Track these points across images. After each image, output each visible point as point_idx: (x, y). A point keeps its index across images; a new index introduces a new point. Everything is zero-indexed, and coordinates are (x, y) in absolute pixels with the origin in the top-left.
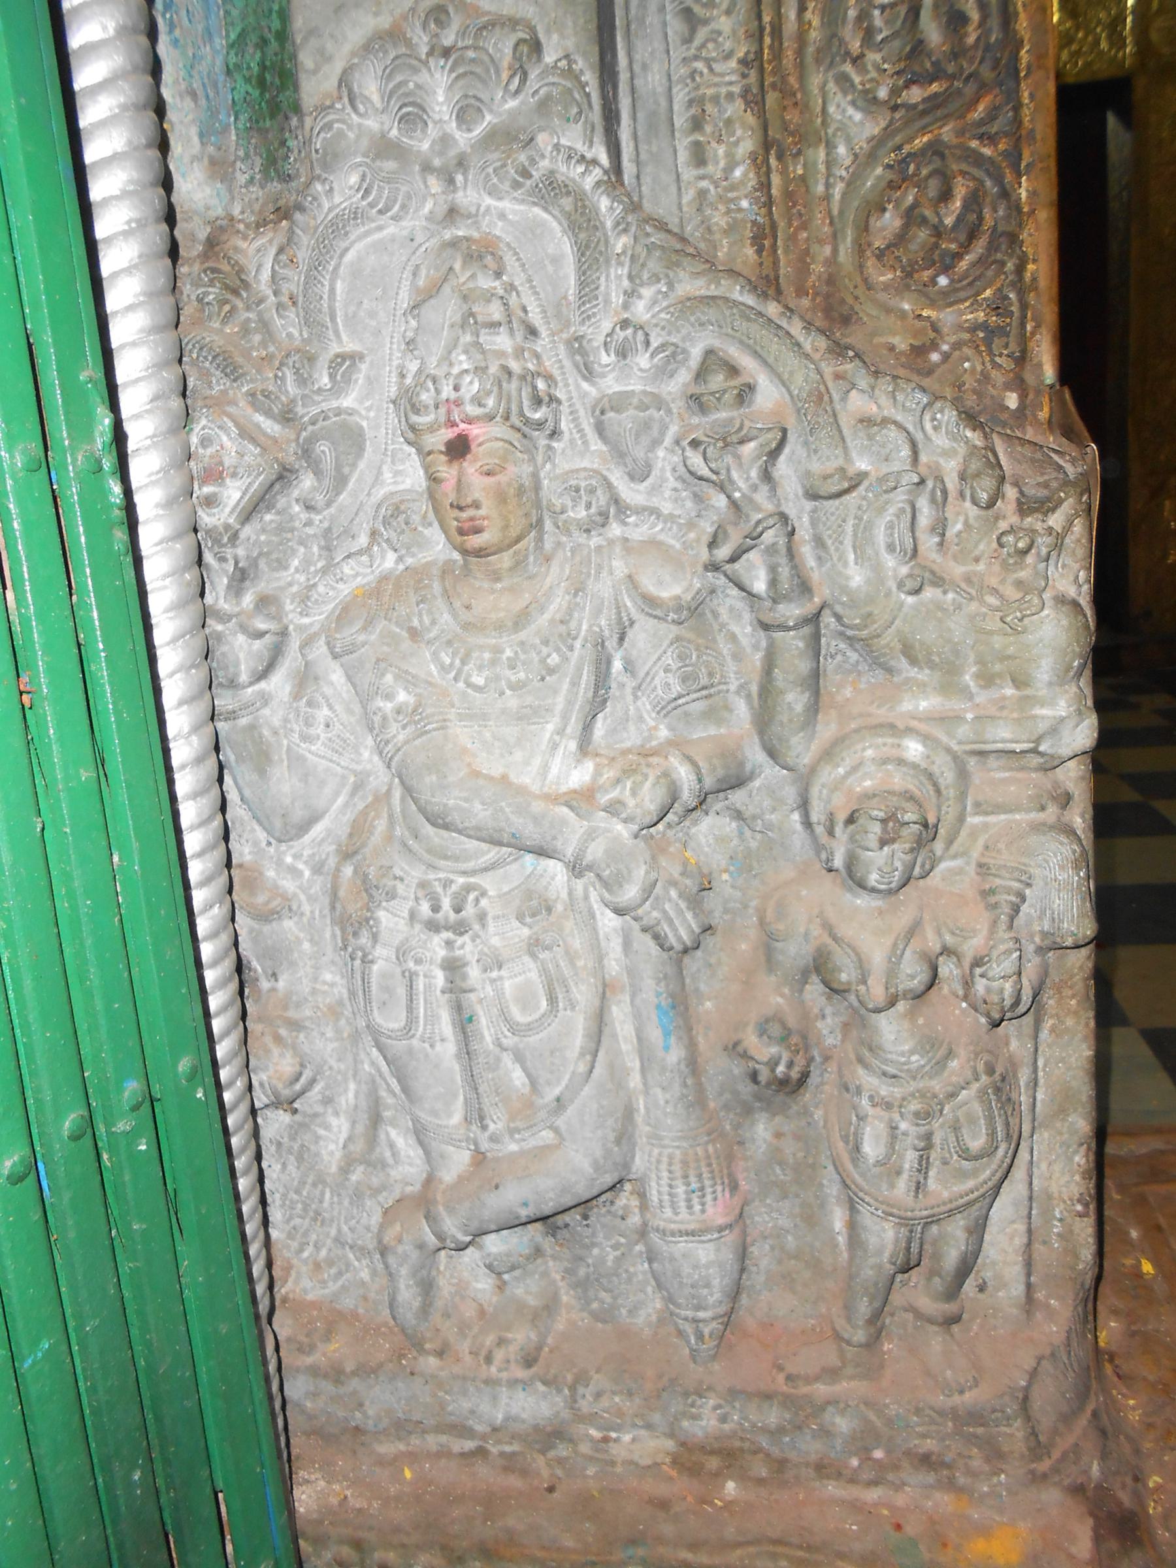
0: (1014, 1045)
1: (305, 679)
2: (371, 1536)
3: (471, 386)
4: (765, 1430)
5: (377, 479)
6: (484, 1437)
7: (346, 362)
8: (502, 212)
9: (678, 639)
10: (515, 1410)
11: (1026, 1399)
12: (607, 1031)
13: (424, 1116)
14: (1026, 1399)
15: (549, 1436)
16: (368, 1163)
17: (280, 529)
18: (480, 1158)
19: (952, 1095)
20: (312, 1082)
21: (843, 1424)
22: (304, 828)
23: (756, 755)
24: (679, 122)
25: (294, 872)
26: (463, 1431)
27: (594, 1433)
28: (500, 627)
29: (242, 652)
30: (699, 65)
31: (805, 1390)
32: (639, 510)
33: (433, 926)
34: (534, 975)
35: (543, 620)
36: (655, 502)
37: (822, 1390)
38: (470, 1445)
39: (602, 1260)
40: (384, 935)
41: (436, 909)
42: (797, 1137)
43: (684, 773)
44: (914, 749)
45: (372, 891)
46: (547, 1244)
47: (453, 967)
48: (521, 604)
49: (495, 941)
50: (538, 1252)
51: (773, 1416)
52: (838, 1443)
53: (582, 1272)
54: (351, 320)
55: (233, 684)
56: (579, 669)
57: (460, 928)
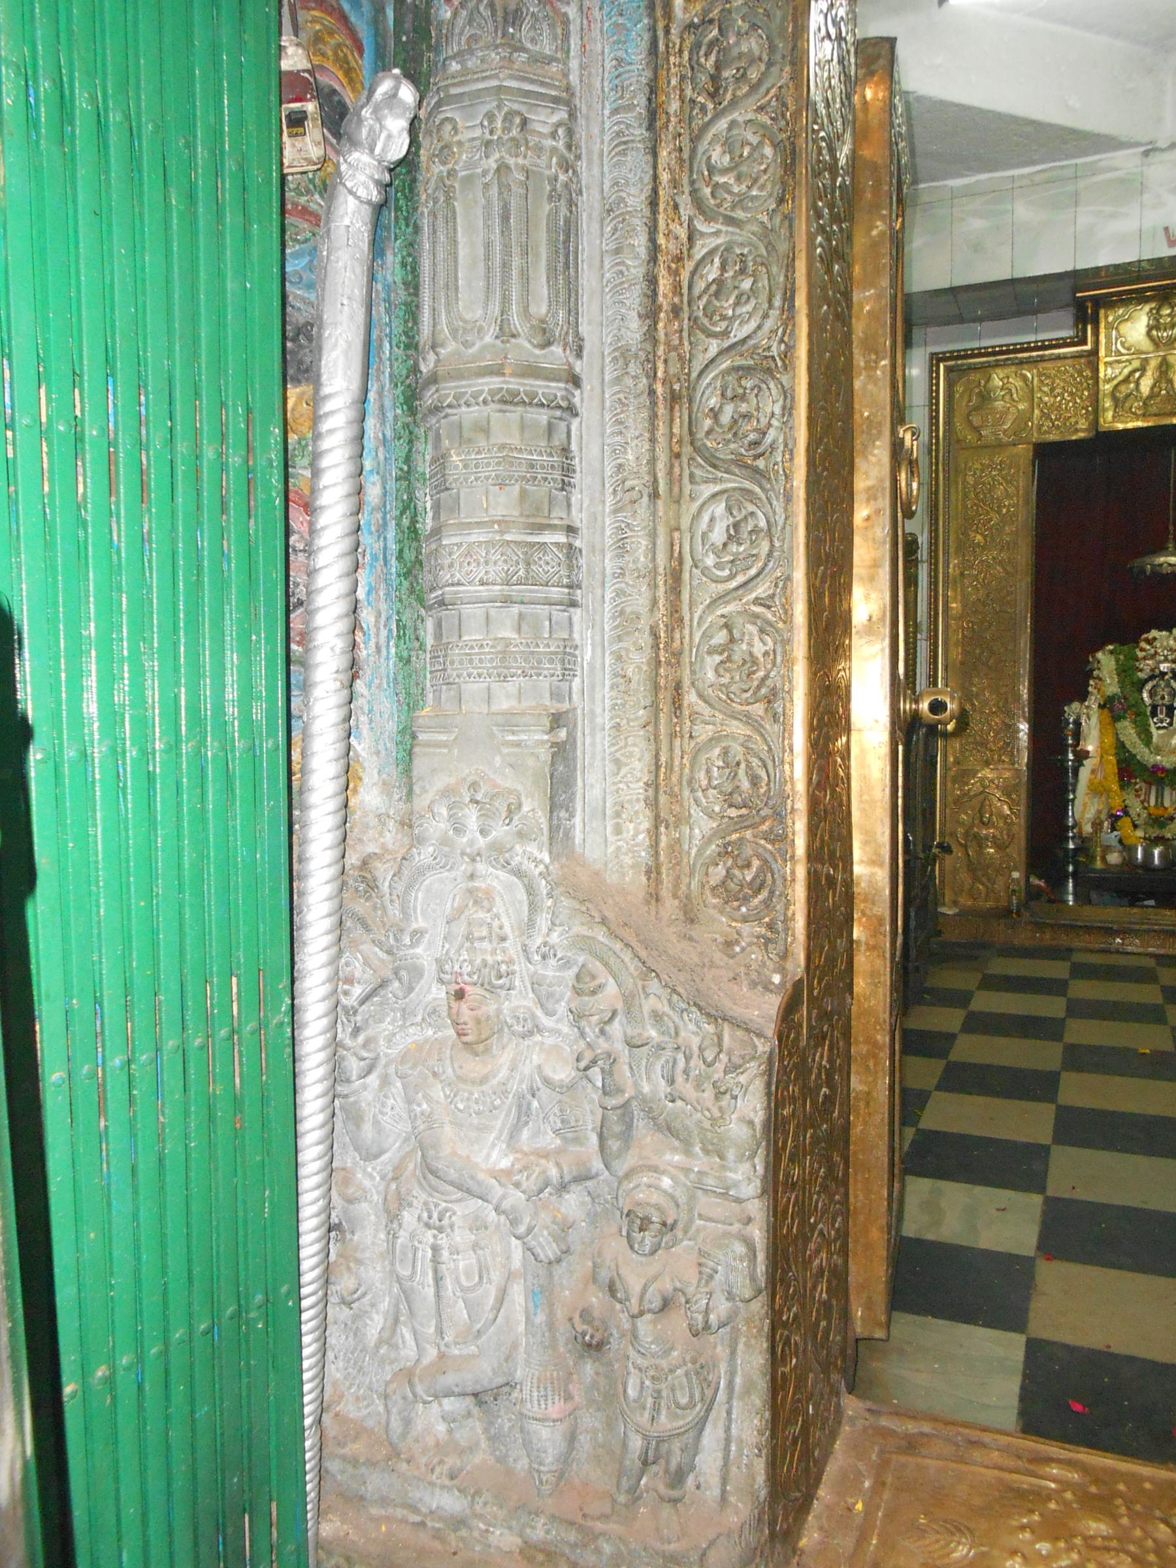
0: (719, 1349)
1: (385, 1081)
2: (355, 1556)
3: (467, 968)
4: (568, 1543)
5: (429, 991)
6: (425, 1516)
7: (418, 935)
8: (494, 878)
9: (560, 1101)
10: (442, 1503)
11: (704, 1554)
12: (507, 1299)
13: (418, 1327)
14: (704, 1554)
15: (459, 1522)
16: (390, 1345)
17: (381, 1004)
18: (442, 1356)
19: (672, 1371)
20: (365, 1294)
21: (607, 1548)
22: (377, 1156)
23: (597, 1165)
24: (608, 812)
25: (372, 1178)
26: (415, 1509)
27: (482, 1526)
28: (473, 1083)
29: (353, 1066)
30: (621, 786)
31: (590, 1523)
32: (551, 1031)
33: (428, 1226)
34: (474, 1261)
35: (495, 1082)
36: (560, 1026)
37: (599, 1526)
38: (418, 1519)
39: (501, 1427)
40: (405, 1225)
41: (430, 1217)
42: (606, 1377)
43: (553, 1172)
44: (666, 1182)
45: (402, 1202)
46: (475, 1411)
47: (435, 1249)
48: (485, 1071)
49: (458, 1239)
50: (469, 1414)
51: (572, 1536)
52: (604, 1559)
53: (493, 1431)
54: (424, 912)
55: (348, 1081)
56: (510, 1109)
57: (440, 1230)
